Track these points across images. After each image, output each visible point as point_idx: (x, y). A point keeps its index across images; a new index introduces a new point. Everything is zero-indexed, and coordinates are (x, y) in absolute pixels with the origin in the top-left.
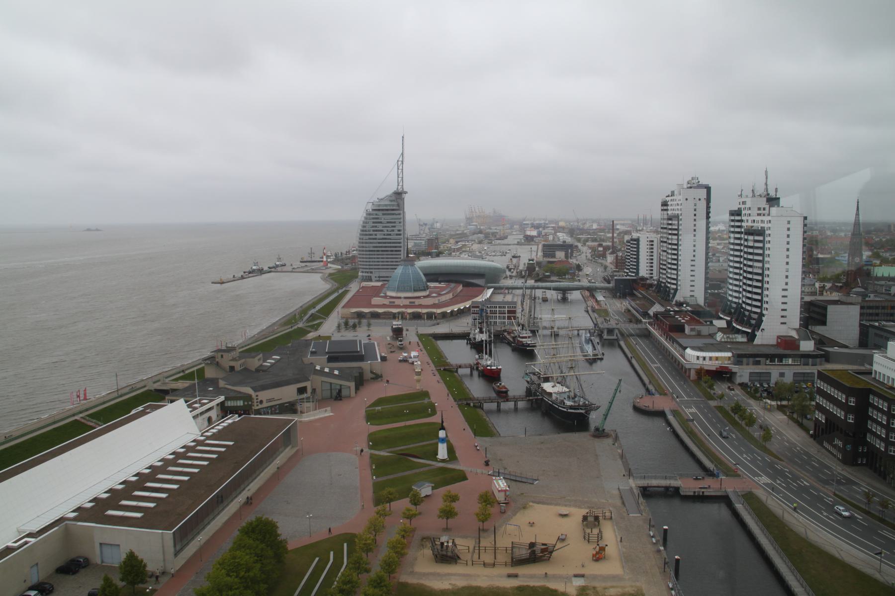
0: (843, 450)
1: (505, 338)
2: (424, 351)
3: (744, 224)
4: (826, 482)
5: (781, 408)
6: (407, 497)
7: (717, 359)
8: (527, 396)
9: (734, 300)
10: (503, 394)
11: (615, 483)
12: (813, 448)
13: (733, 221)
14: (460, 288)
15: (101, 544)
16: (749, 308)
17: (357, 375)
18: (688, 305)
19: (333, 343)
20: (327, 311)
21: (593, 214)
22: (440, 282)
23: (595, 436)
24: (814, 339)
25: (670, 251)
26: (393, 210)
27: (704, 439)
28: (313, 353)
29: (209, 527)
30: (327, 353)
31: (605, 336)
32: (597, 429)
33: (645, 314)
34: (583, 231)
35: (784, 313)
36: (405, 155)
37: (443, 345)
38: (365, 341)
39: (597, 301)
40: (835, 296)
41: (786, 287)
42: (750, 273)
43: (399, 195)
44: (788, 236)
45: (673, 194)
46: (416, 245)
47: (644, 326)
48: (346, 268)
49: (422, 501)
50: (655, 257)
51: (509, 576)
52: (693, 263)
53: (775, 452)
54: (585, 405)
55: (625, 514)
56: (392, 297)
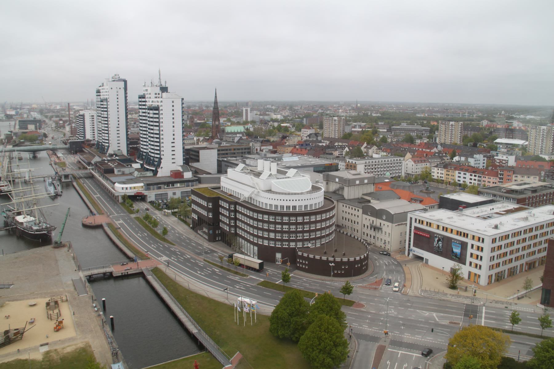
3: (147, 103)
4: (199, 254)
5: (174, 214)
7: (135, 188)
8: (5, 227)
9: (145, 151)
13: (140, 101)
16: (153, 155)
18: (116, 155)
21: (56, 98)
23: (55, 248)
27: (127, 239)
31: (63, 180)
33: (89, 164)
34: (50, 111)
39: (58, 157)
40: (205, 144)
41: (173, 141)
42: (152, 133)
44: (173, 110)
45: (103, 85)
50: (95, 127)
52: (118, 129)
54: (47, 228)
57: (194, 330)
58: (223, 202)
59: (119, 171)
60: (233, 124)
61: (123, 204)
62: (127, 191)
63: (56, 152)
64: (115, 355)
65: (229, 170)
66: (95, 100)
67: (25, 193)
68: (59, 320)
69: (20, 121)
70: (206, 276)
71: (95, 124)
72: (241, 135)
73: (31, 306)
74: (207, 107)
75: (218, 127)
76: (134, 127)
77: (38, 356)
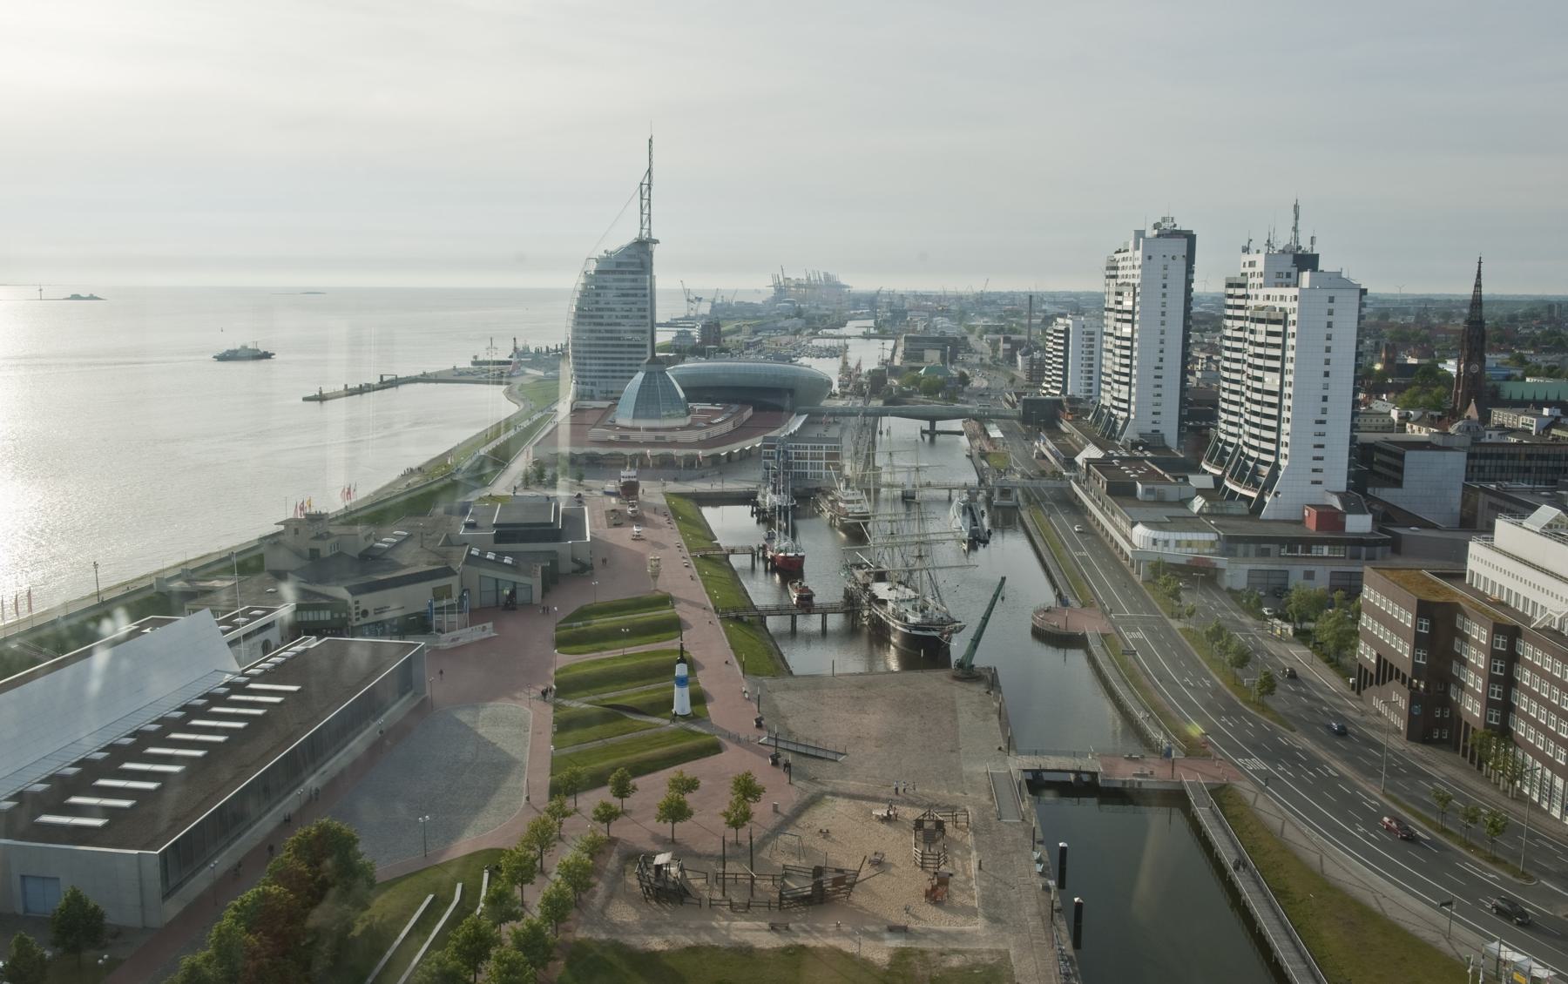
3: (1250, 303)
6: (605, 784)
7: (1189, 544)
8: (846, 604)
10: (806, 603)
14: (749, 412)
15: (23, 877)
16: (1254, 454)
22: (714, 403)
24: (1371, 511)
29: (238, 842)
30: (495, 526)
32: (960, 665)
35: (1318, 464)
36: (654, 174)
37: (708, 513)
41: (1323, 417)
43: (642, 250)
47: (1065, 484)
52: (1159, 373)
62: (1166, 550)
65: (1503, 527)
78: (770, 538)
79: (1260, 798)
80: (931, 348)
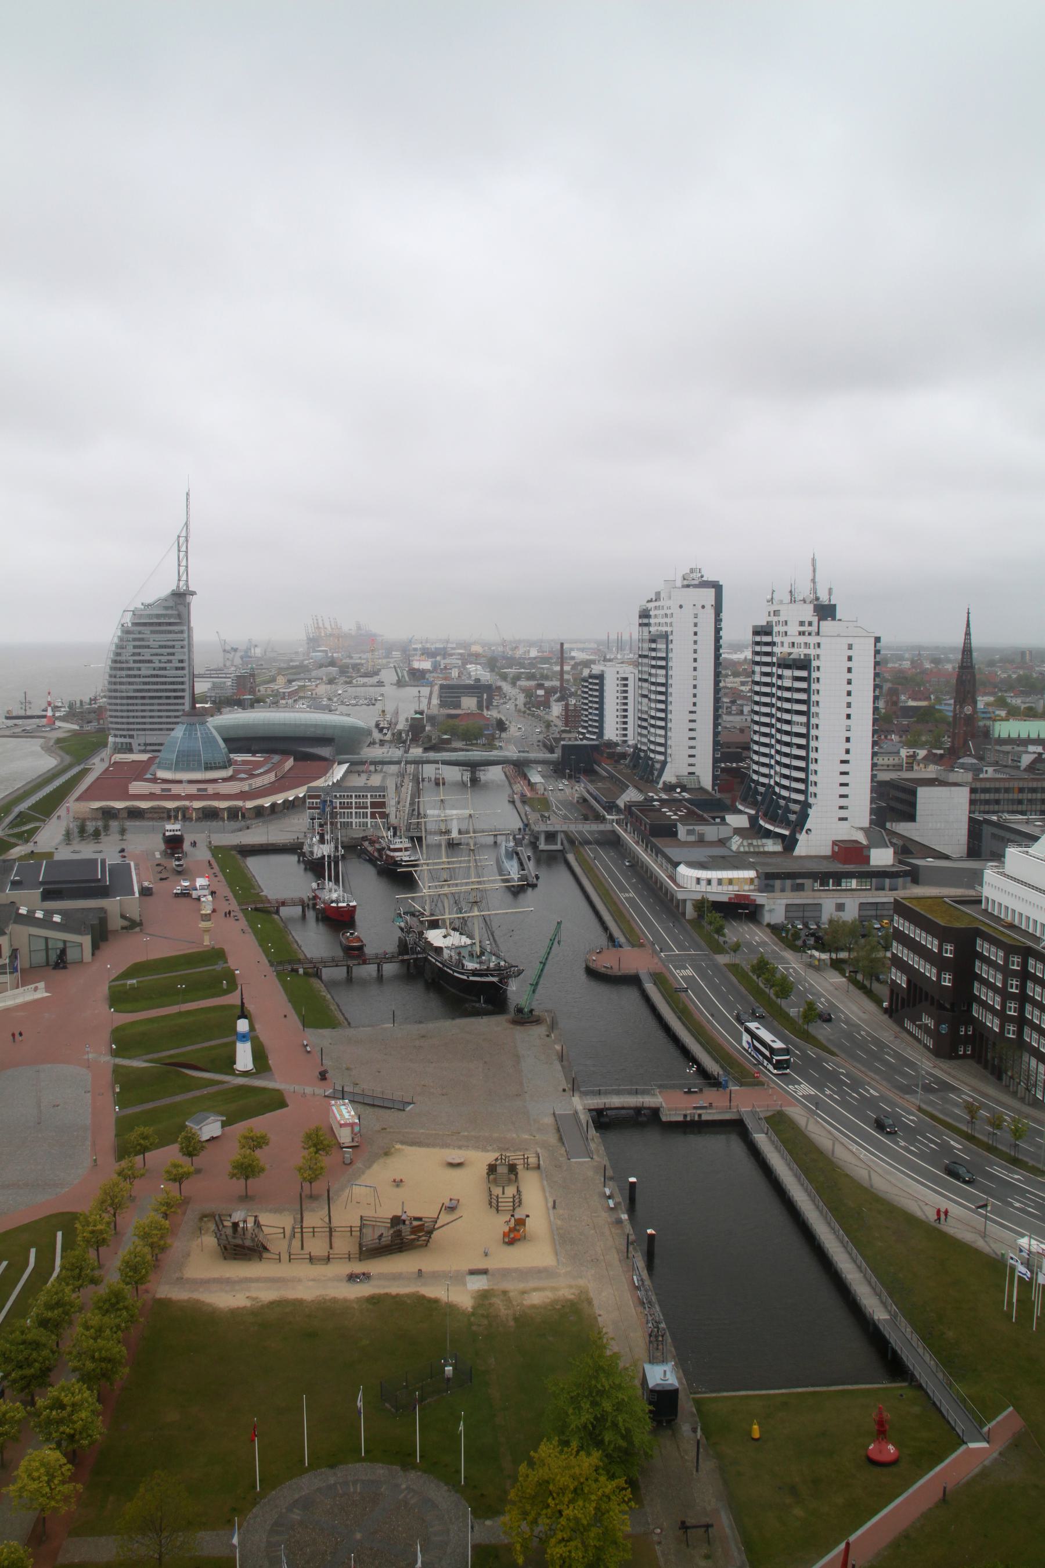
0: (934, 1034)
1: (365, 851)
2: (221, 877)
3: (776, 649)
4: (906, 1090)
5: (837, 965)
6: (175, 1141)
7: (731, 881)
8: (401, 953)
10: (355, 953)
11: (551, 1103)
12: (885, 1031)
13: (758, 643)
14: (290, 762)
16: (785, 793)
17: (96, 922)
18: (684, 789)
19: (55, 866)
20: (48, 807)
22: (254, 753)
23: (515, 1022)
24: (893, 845)
25: (653, 696)
26: (170, 624)
28: (16, 884)
30: (42, 883)
31: (542, 846)
33: (611, 807)
34: (511, 662)
36: (191, 526)
37: (254, 865)
38: (113, 859)
40: (931, 771)
41: (846, 757)
42: (787, 733)
43: (180, 598)
45: (658, 597)
46: (215, 686)
47: (608, 827)
48: (88, 728)
49: (203, 1148)
50: (630, 707)
51: (352, 1278)
52: (693, 717)
53: (824, 1042)
54: (498, 968)
55: (563, 1159)
56: (165, 781)
57: (877, 1310)
58: (986, 945)
59: (690, 832)
60: (1014, 713)
61: (697, 923)
62: (709, 889)
63: (526, 770)
64: (654, 1338)
65: (1012, 853)
66: (636, 636)
67: (452, 873)
68: (517, 1216)
69: (442, 687)
70: (921, 1156)
71: (630, 701)
72: (1040, 749)
73: (452, 1165)
74: (936, 661)
75: (970, 720)
76: (729, 713)
77: (462, 1296)
78: (321, 887)
79: (811, 1121)
80: (467, 695)
